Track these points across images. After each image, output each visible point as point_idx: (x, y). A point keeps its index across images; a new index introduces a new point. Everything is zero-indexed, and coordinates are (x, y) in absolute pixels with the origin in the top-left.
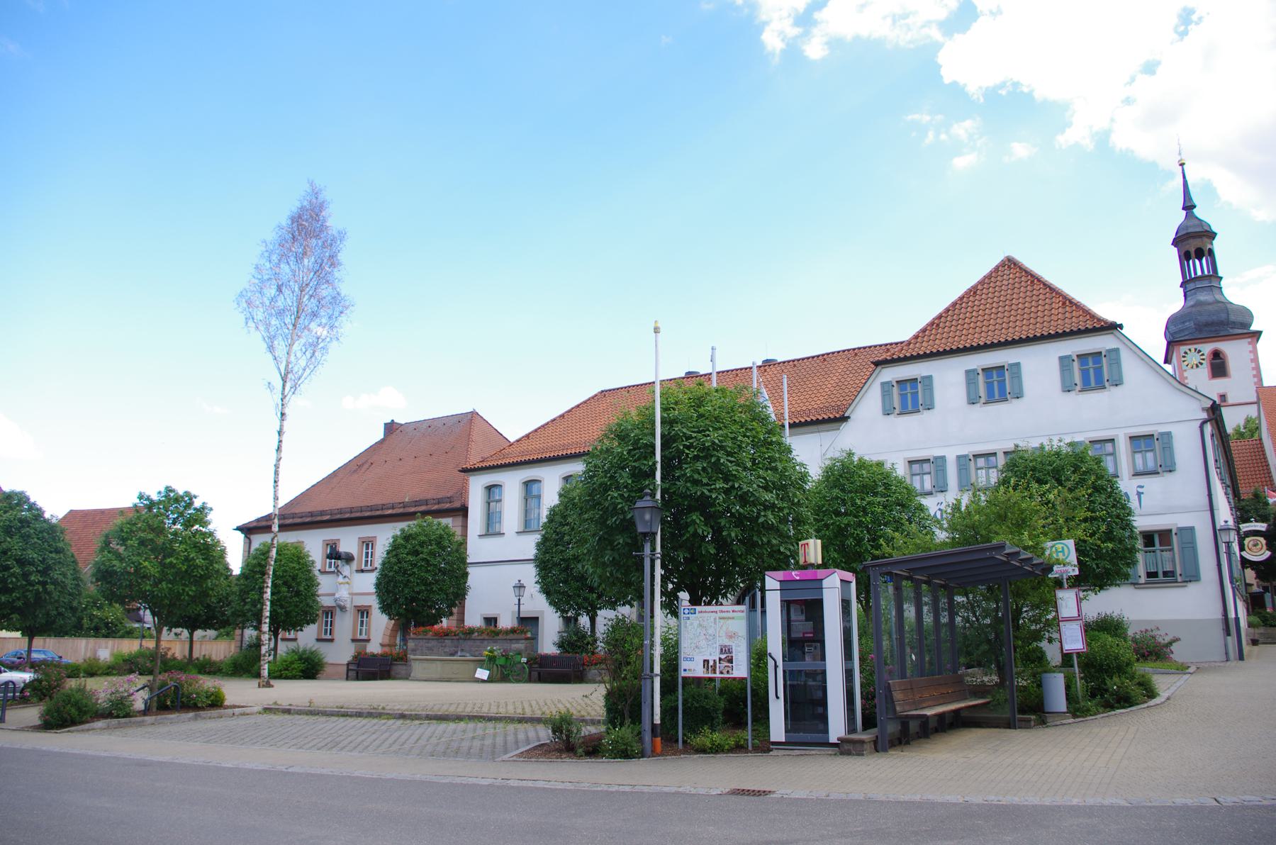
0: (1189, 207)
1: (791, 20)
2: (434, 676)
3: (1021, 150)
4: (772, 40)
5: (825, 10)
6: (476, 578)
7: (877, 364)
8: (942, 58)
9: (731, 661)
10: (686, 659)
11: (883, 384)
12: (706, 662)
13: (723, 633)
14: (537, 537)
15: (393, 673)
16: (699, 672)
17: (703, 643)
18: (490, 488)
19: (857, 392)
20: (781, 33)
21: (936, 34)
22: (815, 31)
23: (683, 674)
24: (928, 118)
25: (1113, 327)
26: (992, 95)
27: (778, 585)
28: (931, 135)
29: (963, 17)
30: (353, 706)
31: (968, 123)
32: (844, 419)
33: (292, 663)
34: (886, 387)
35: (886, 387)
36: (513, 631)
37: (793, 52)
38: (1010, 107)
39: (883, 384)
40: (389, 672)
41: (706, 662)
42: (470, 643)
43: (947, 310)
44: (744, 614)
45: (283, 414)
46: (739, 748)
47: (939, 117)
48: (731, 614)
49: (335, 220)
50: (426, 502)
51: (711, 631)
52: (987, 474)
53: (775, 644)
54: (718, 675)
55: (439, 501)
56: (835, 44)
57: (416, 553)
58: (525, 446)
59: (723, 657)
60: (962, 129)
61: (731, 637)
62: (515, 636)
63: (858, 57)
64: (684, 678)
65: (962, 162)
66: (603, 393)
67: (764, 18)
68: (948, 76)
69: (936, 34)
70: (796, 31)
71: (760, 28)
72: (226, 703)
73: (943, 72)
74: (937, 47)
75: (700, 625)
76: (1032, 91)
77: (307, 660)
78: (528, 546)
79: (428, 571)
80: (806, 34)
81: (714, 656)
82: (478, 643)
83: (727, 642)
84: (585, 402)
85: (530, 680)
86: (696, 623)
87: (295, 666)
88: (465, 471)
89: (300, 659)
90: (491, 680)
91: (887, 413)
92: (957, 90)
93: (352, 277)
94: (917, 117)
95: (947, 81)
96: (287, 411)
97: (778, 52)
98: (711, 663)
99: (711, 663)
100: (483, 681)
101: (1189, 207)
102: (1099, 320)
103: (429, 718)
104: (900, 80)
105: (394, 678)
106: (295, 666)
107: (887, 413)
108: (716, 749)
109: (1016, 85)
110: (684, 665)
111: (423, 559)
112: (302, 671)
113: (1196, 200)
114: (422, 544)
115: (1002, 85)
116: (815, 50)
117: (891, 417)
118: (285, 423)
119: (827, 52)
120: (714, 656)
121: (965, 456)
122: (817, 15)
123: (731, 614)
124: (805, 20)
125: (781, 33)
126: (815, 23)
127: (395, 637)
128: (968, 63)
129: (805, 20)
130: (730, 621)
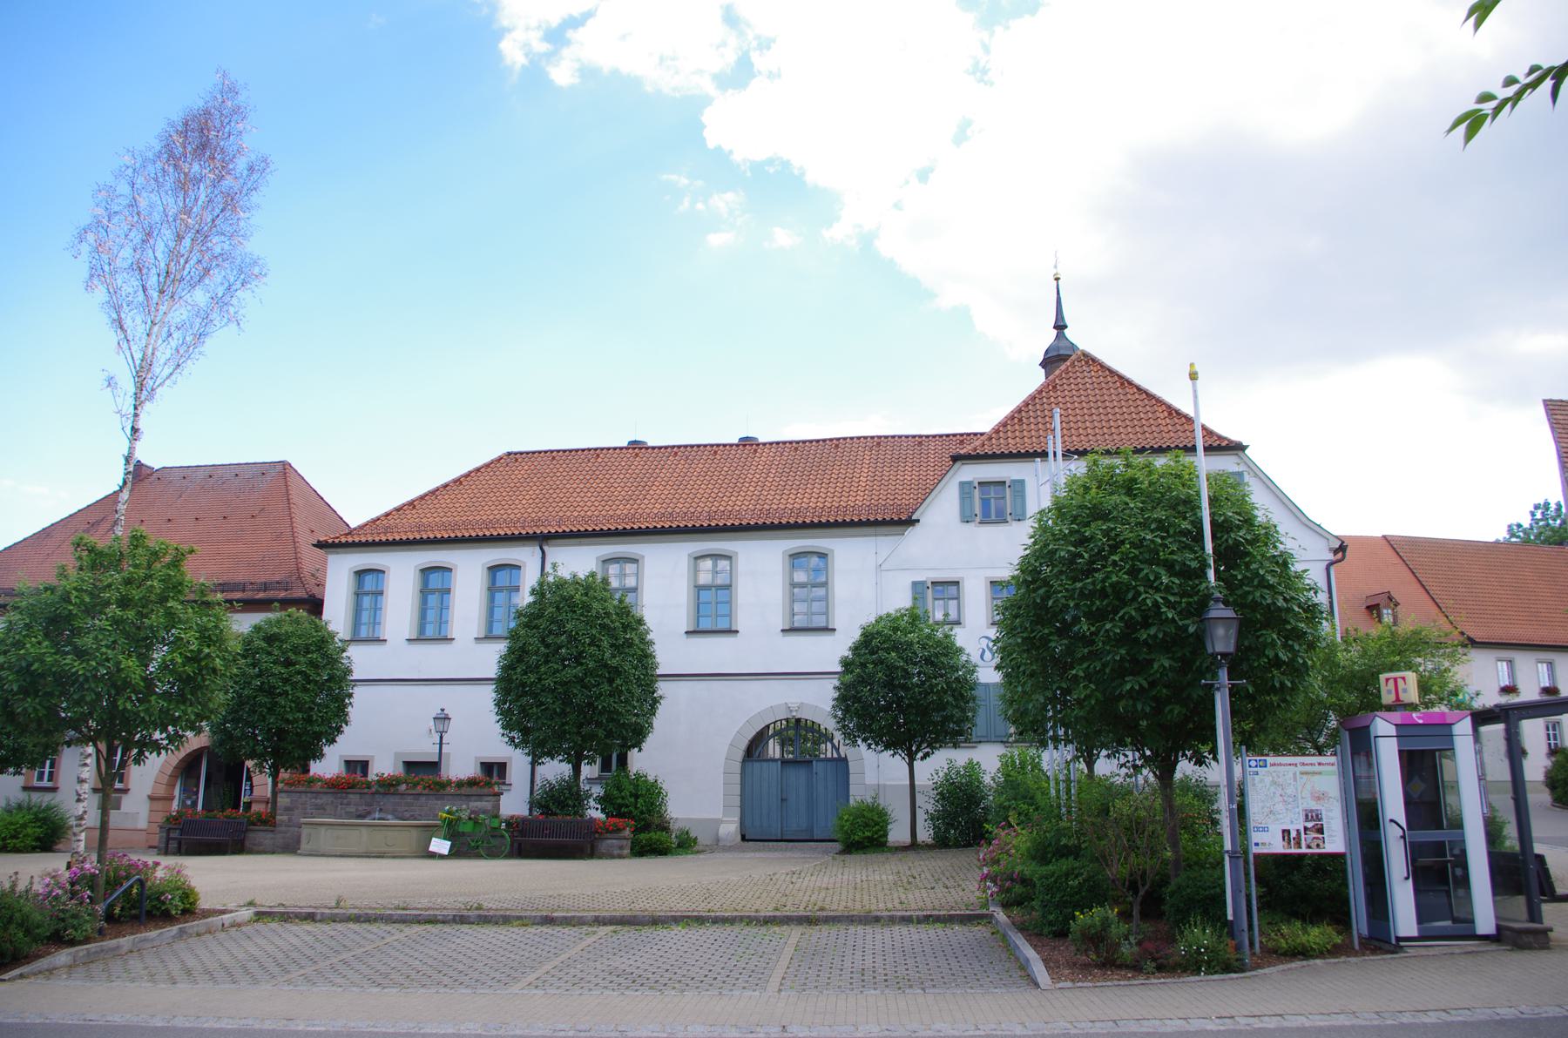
0: (1060, 326)
1: (540, 34)
2: (355, 849)
3: (783, 237)
4: (512, 51)
5: (581, 29)
6: (361, 702)
7: (956, 459)
8: (708, 116)
9: (1321, 831)
10: (1258, 829)
11: (962, 484)
12: (1286, 832)
13: (1306, 793)
14: (501, 647)
15: (247, 844)
16: (1278, 846)
17: (1280, 807)
18: (360, 574)
19: (926, 492)
20: (526, 47)
21: (710, 88)
22: (565, 52)
23: (1255, 850)
24: (686, 181)
25: (1237, 448)
26: (758, 168)
27: (1392, 730)
28: (686, 204)
29: (740, 75)
30: (303, 903)
31: (730, 196)
32: (911, 522)
33: (24, 826)
34: (965, 487)
35: (965, 487)
36: (472, 782)
37: (535, 73)
38: (777, 186)
39: (962, 484)
40: (242, 842)
41: (1286, 832)
42: (393, 799)
43: (1026, 404)
44: (1335, 768)
45: (135, 430)
46: (1335, 951)
47: (700, 183)
48: (1317, 768)
49: (252, 139)
50: (242, 587)
51: (1289, 791)
52: (946, 607)
53: (1393, 805)
54: (1304, 850)
55: (266, 587)
56: (588, 73)
57: (288, 663)
58: (412, 518)
59: (1309, 825)
60: (724, 201)
61: (1319, 799)
62: (475, 790)
63: (609, 93)
64: (1257, 856)
65: (715, 240)
66: (513, 457)
67: (505, 23)
68: (712, 138)
69: (710, 88)
70: (543, 47)
71: (501, 33)
72: (203, 904)
73: (706, 133)
74: (706, 101)
75: (1274, 783)
76: (803, 174)
77: (45, 821)
78: (489, 659)
79: (305, 690)
80: (550, 56)
81: (1297, 824)
82: (409, 799)
83: (1313, 805)
84: (487, 465)
85: (510, 856)
86: (1268, 780)
87: (29, 831)
88: (321, 545)
89: (37, 819)
90: (455, 854)
91: (966, 519)
92: (721, 157)
93: (267, 227)
94: (674, 177)
95: (711, 144)
96: (141, 425)
97: (518, 67)
98: (1293, 834)
99: (1293, 834)
100: (442, 857)
101: (1060, 326)
102: (1220, 437)
103: (600, 921)
104: (648, 137)
105: (251, 852)
106: (29, 831)
107: (966, 519)
108: (1301, 953)
109: (786, 164)
110: (1255, 837)
111: (300, 672)
112: (38, 839)
113: (1068, 321)
114: (295, 650)
115: (770, 162)
116: (562, 74)
117: (971, 525)
118: (138, 444)
119: (577, 81)
120: (1297, 824)
121: (923, 583)
122: (570, 34)
123: (1317, 768)
124: (557, 36)
125: (526, 47)
126: (568, 43)
127: (172, 786)
128: (734, 127)
129: (557, 36)
130: (1316, 777)
